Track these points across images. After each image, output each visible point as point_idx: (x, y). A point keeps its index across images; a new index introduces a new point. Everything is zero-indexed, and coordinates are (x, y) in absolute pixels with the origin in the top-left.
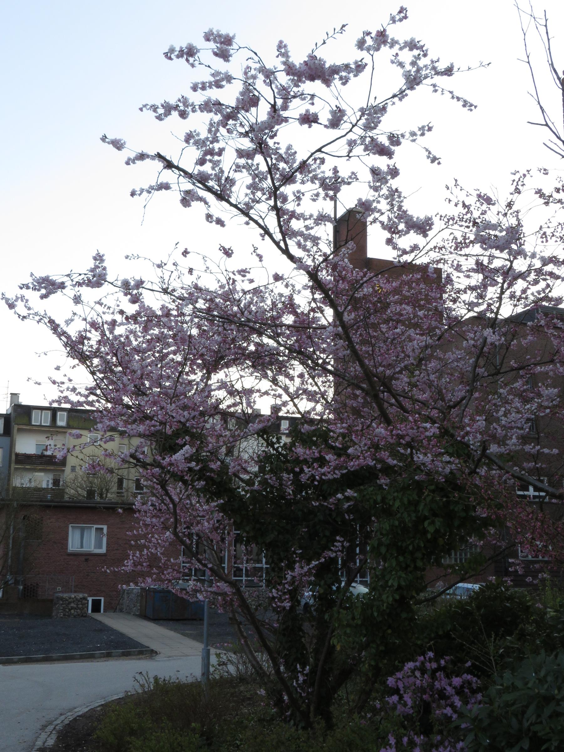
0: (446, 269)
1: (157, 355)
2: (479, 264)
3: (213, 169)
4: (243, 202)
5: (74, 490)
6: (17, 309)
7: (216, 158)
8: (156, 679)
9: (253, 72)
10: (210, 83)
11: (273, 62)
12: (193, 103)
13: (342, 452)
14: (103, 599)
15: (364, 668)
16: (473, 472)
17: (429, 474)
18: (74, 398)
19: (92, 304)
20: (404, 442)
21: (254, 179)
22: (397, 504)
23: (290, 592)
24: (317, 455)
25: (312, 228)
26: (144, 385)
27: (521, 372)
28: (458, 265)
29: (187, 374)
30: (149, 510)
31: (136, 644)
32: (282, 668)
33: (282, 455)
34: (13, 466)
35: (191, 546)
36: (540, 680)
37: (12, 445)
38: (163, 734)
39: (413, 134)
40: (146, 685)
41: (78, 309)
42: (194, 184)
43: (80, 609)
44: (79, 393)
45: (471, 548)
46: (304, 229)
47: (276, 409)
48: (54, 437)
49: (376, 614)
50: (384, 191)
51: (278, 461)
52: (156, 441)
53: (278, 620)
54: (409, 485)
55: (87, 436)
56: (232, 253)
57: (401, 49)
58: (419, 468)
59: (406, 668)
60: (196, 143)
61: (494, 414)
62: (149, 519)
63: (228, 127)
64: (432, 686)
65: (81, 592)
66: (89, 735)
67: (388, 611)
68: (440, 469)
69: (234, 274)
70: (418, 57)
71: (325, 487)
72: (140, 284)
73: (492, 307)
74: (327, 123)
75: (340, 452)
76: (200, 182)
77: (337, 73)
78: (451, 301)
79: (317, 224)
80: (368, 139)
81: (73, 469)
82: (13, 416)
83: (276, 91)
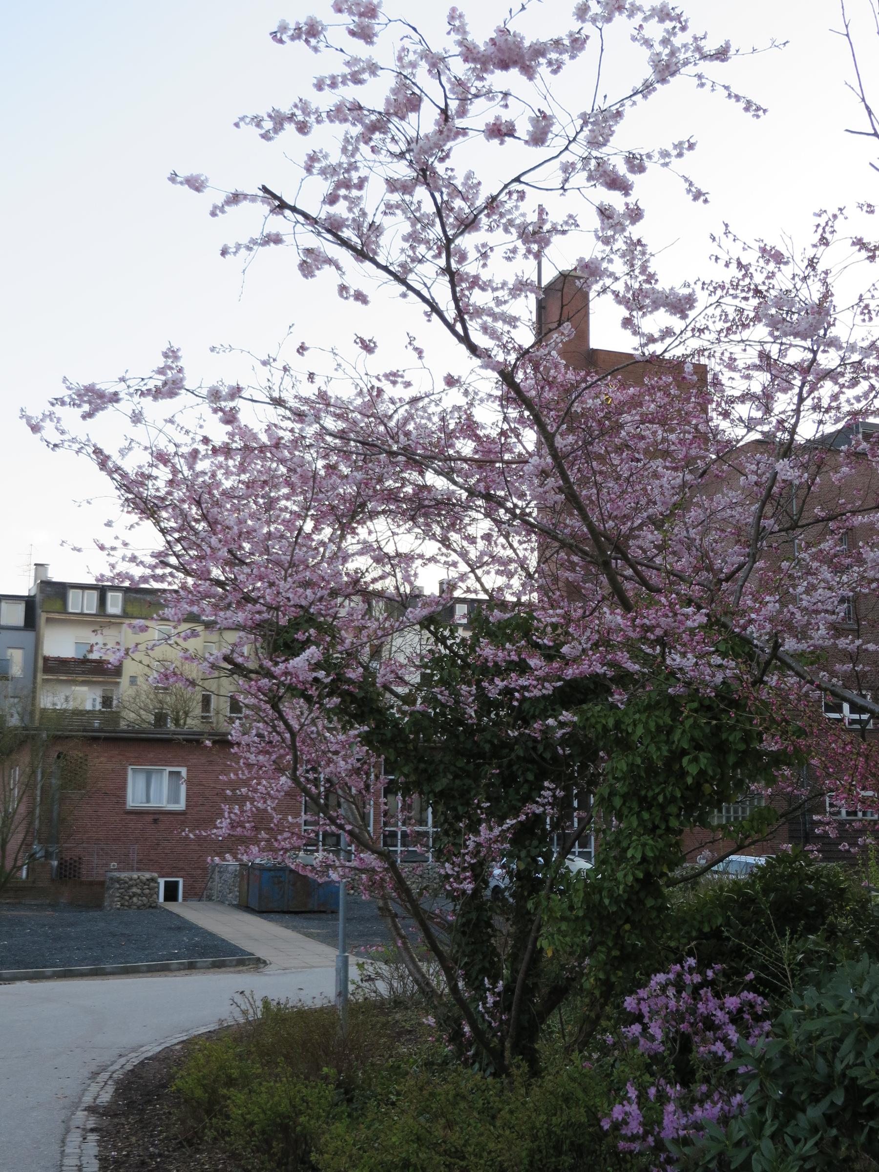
0: (713, 365)
1: (261, 501)
2: (764, 356)
3: (350, 210)
4: (397, 263)
5: (135, 713)
6: (44, 433)
7: (355, 193)
8: (266, 1003)
9: (412, 57)
10: (344, 77)
11: (443, 42)
12: (317, 109)
13: (553, 652)
14: (181, 880)
15: (589, 983)
16: (759, 681)
17: (688, 684)
18: (137, 572)
19: (160, 424)
21: (413, 225)
22: (640, 731)
23: (472, 867)
25: (506, 302)
26: (241, 548)
27: (832, 525)
28: (730, 359)
30: (254, 742)
31: (234, 950)
32: (461, 984)
34: (40, 676)
35: (321, 798)
36: (861, 1000)
37: (38, 644)
38: (278, 1085)
39: (665, 154)
40: (251, 1011)
41: (139, 433)
43: (146, 896)
44: (142, 562)
45: (753, 798)
46: (492, 304)
47: (448, 587)
48: (106, 631)
49: (607, 901)
50: (620, 244)
52: (263, 636)
53: (454, 910)
55: (155, 631)
57: (646, 19)
58: (672, 674)
59: (652, 983)
60: (323, 172)
61: (791, 590)
62: (252, 757)
63: (372, 144)
64: (693, 1011)
65: (148, 870)
66: (164, 1086)
67: (626, 896)
68: (707, 678)
69: (379, 380)
70: (672, 32)
72: (236, 392)
73: (786, 425)
74: (527, 138)
75: (551, 654)
76: (329, 231)
77: (543, 55)
78: (720, 414)
81: (133, 680)
82: (38, 599)
83: (448, 86)
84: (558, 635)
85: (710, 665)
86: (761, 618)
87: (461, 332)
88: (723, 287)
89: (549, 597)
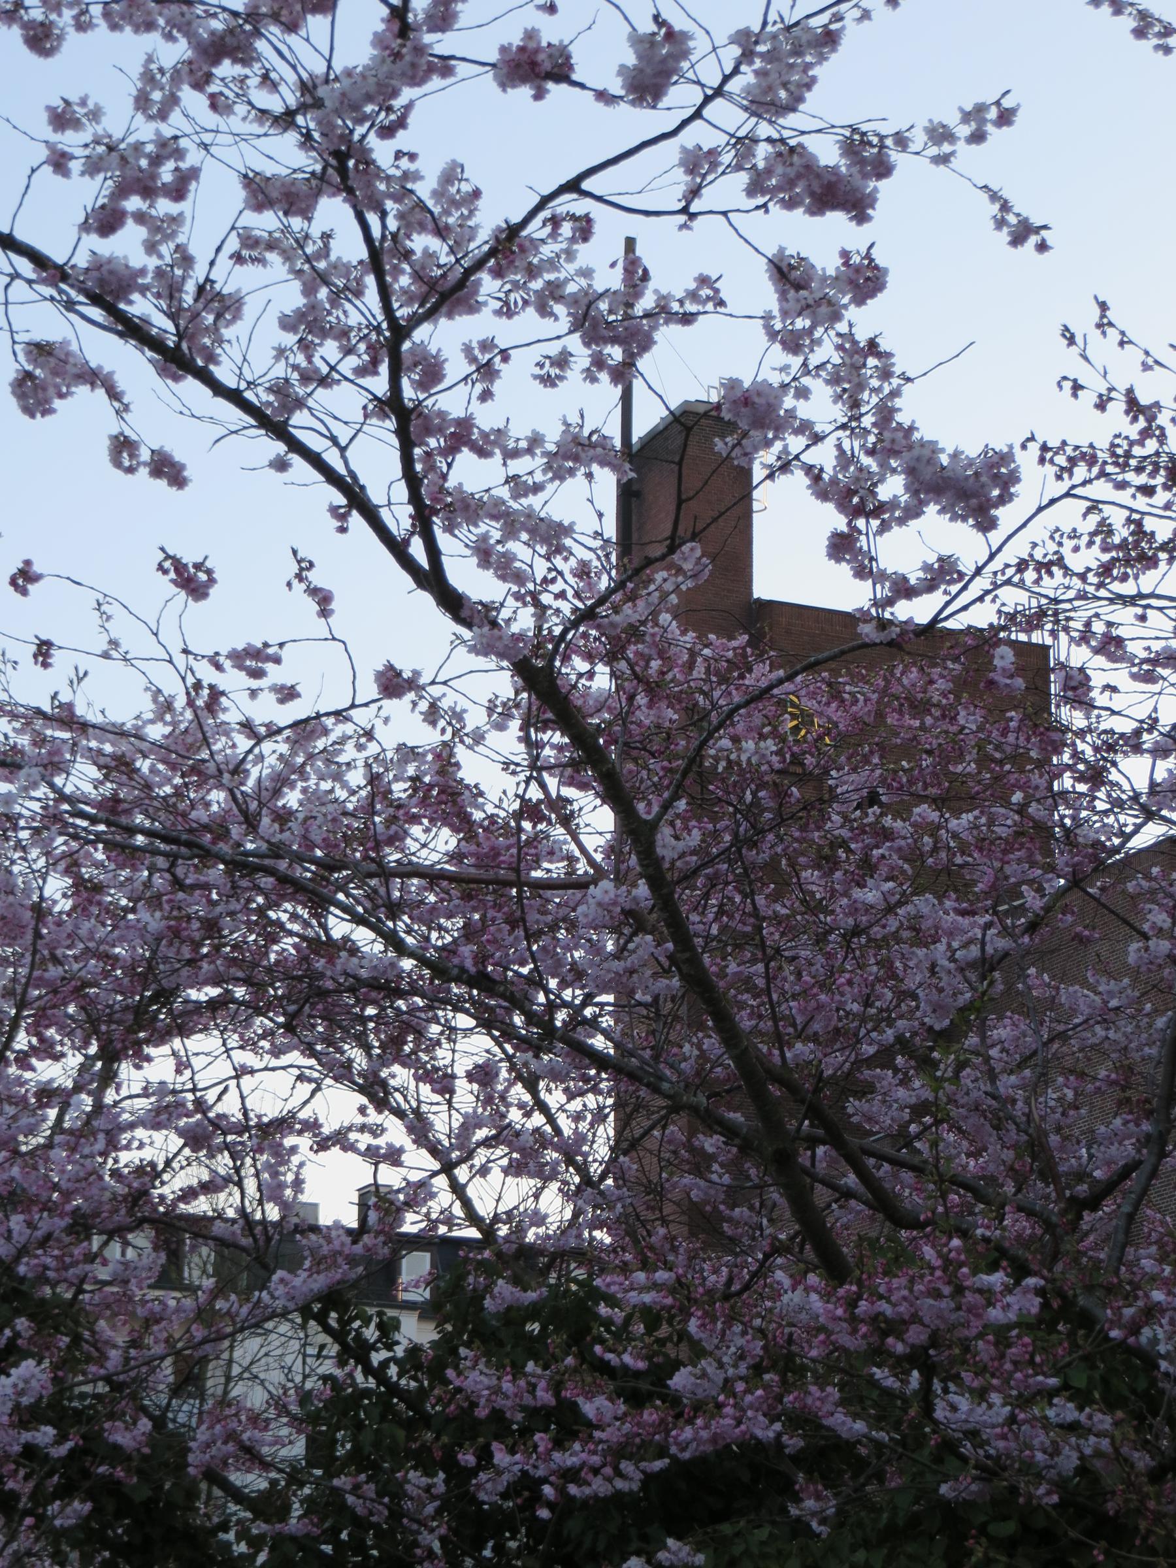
3: (151, 248)
7: (164, 206)
13: (644, 1386)
17: (990, 1471)
20: (900, 1348)
21: (309, 290)
24: (544, 1396)
25: (537, 488)
29: (23, 1060)
33: (403, 1394)
39: (940, 134)
46: (504, 493)
47: (377, 1204)
50: (826, 352)
51: (383, 1418)
56: (212, 581)
58: (949, 1447)
63: (213, 88)
68: (1039, 1456)
69: (219, 667)
71: (574, 1526)
74: (616, 87)
75: (637, 1391)
76: (96, 300)
79: (560, 475)
80: (763, 151)
84: (662, 1342)
88: (1091, 460)
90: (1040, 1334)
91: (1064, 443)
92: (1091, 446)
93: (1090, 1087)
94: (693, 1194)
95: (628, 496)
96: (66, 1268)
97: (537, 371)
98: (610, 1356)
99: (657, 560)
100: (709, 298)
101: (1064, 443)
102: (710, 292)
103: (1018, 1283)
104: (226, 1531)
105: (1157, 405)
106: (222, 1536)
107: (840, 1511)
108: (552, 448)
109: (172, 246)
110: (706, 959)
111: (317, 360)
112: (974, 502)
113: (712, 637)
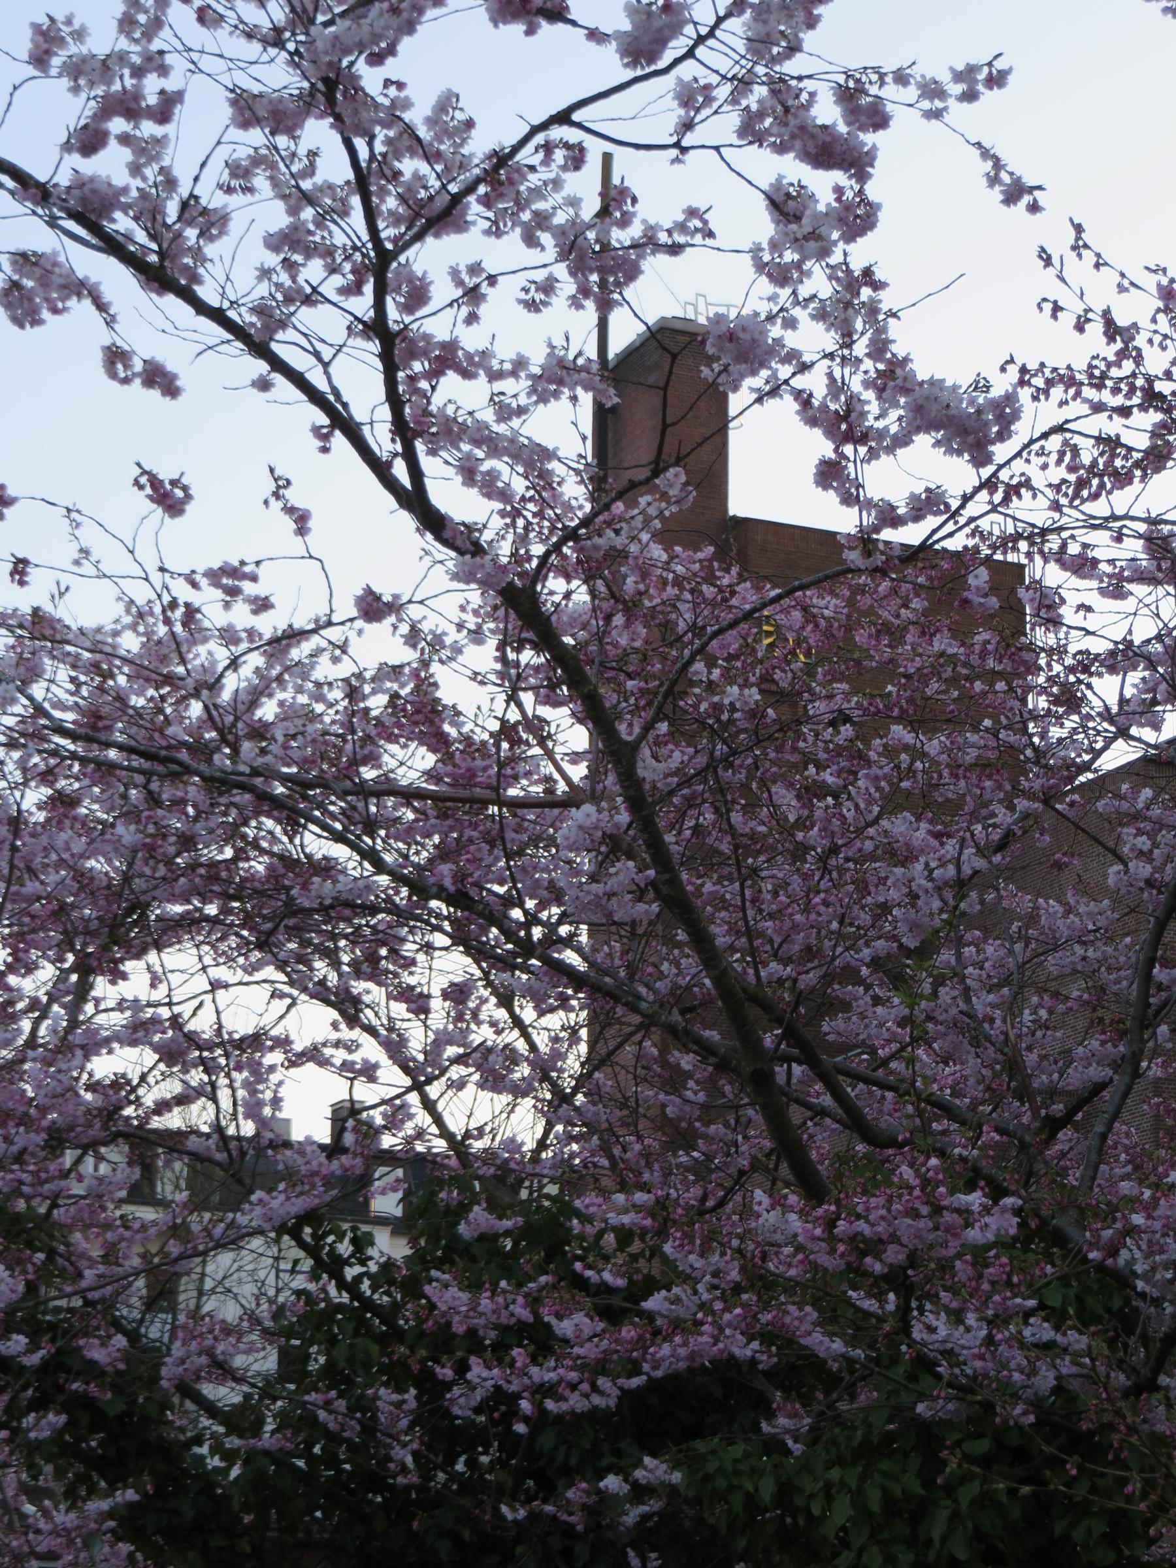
3: (135, 170)
7: (148, 128)
13: (617, 1302)
17: (964, 1389)
20: (878, 1267)
21: (293, 211)
22: (842, 1512)
25: (521, 411)
39: (932, 90)
42: (52, 223)
46: (488, 415)
47: (346, 1115)
50: (818, 283)
51: (356, 1333)
54: (889, 1438)
56: (188, 497)
58: (923, 1364)
60: (76, 70)
68: (1017, 1376)
69: (195, 585)
71: (547, 1440)
75: (613, 1308)
84: (634, 1258)
85: (1022, 1345)
86: (1157, 1225)
87: (405, 479)
88: (1069, 381)
89: (611, 1158)
90: (1016, 1253)
91: (1042, 365)
92: (1069, 367)
93: (1061, 1008)
94: (668, 1110)
95: (602, 414)
96: (42, 1183)
97: (522, 296)
98: (589, 1273)
99: (641, 483)
100: (697, 230)
101: (1042, 365)
102: (699, 224)
103: (996, 1202)
104: (200, 1445)
105: (1135, 326)
106: (197, 1450)
107: (813, 1428)
108: (537, 370)
109: (156, 167)
110: (684, 876)
111: (301, 280)
112: (971, 439)
113: (678, 549)
